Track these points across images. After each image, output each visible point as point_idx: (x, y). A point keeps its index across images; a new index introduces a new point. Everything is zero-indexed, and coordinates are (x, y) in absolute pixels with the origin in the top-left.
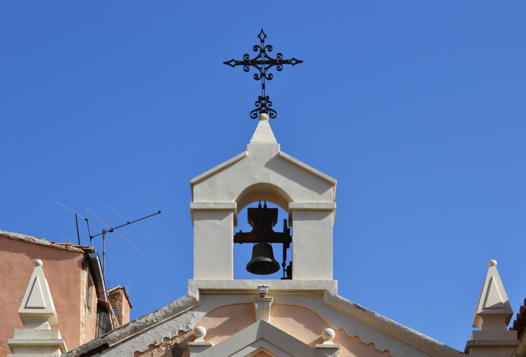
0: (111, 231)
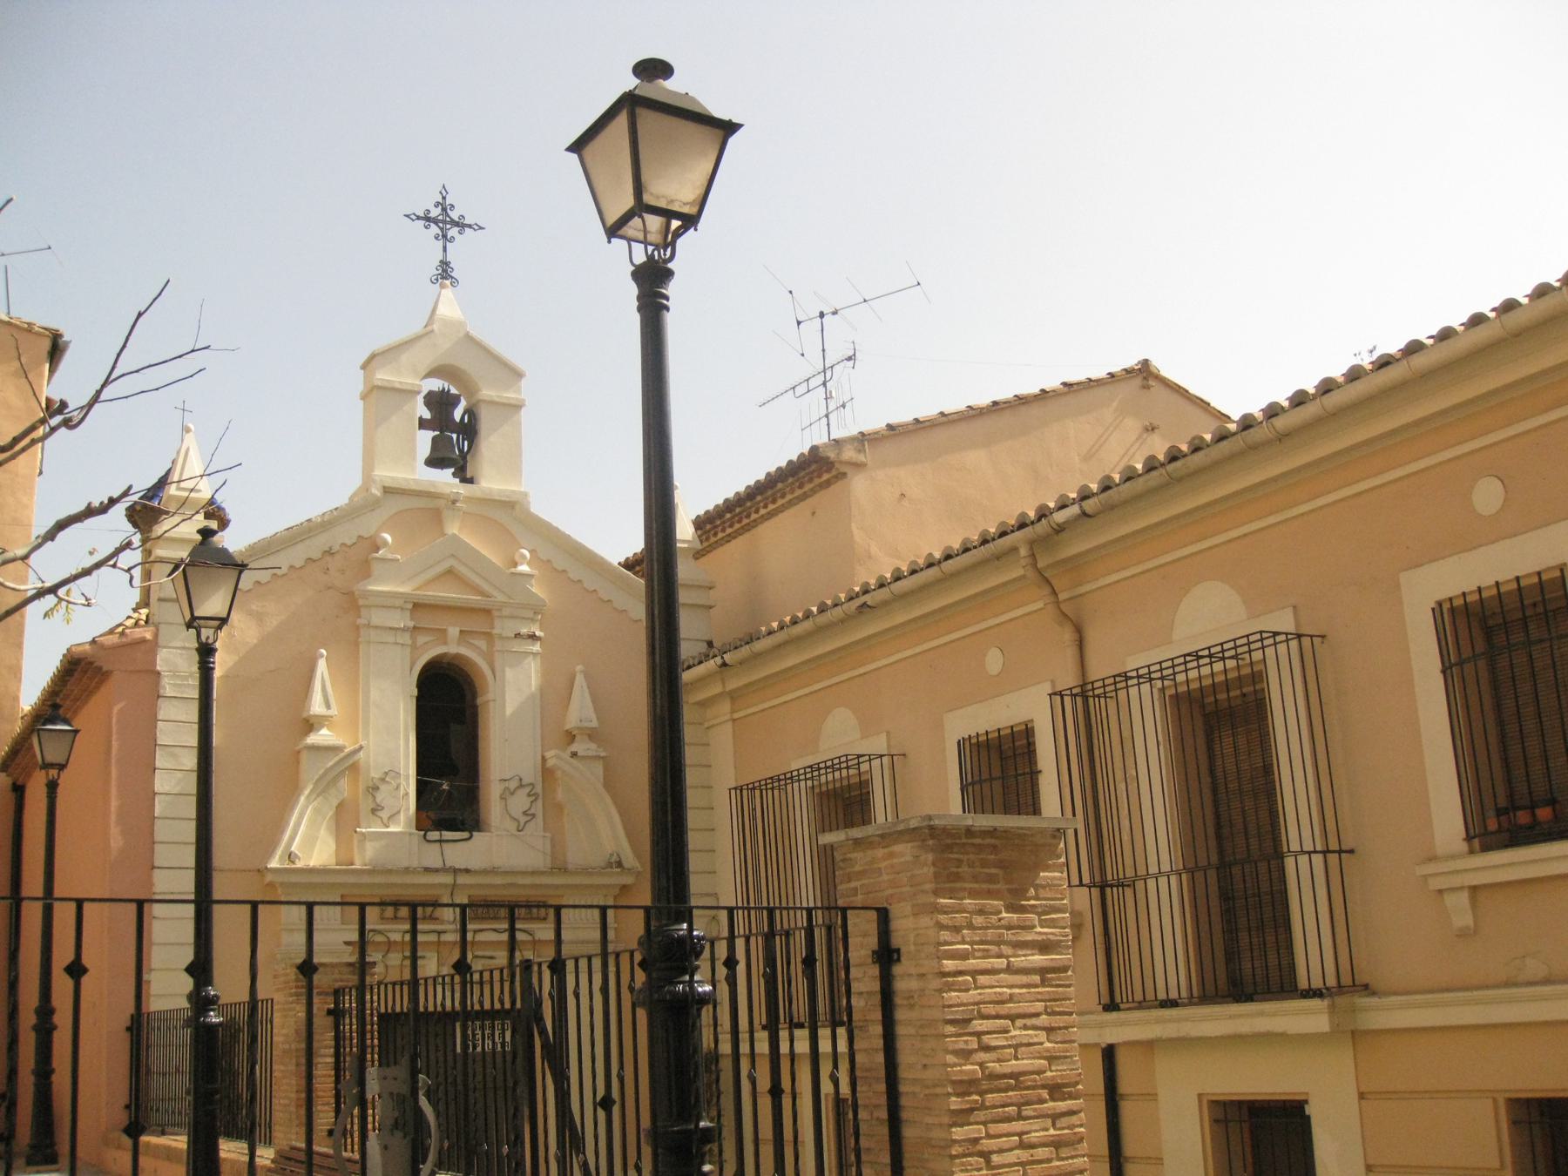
0: (835, 313)
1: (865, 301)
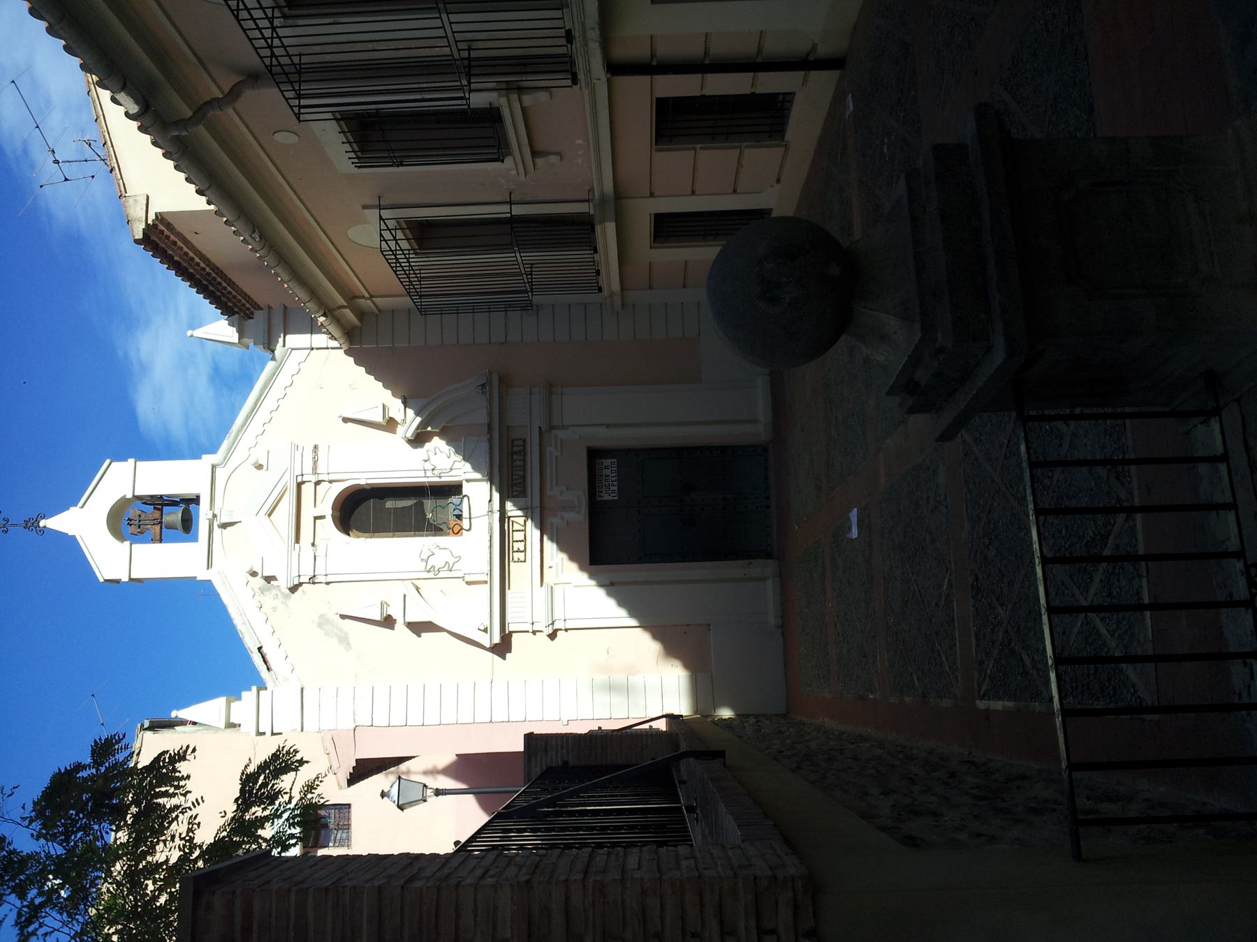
1: (37, 127)
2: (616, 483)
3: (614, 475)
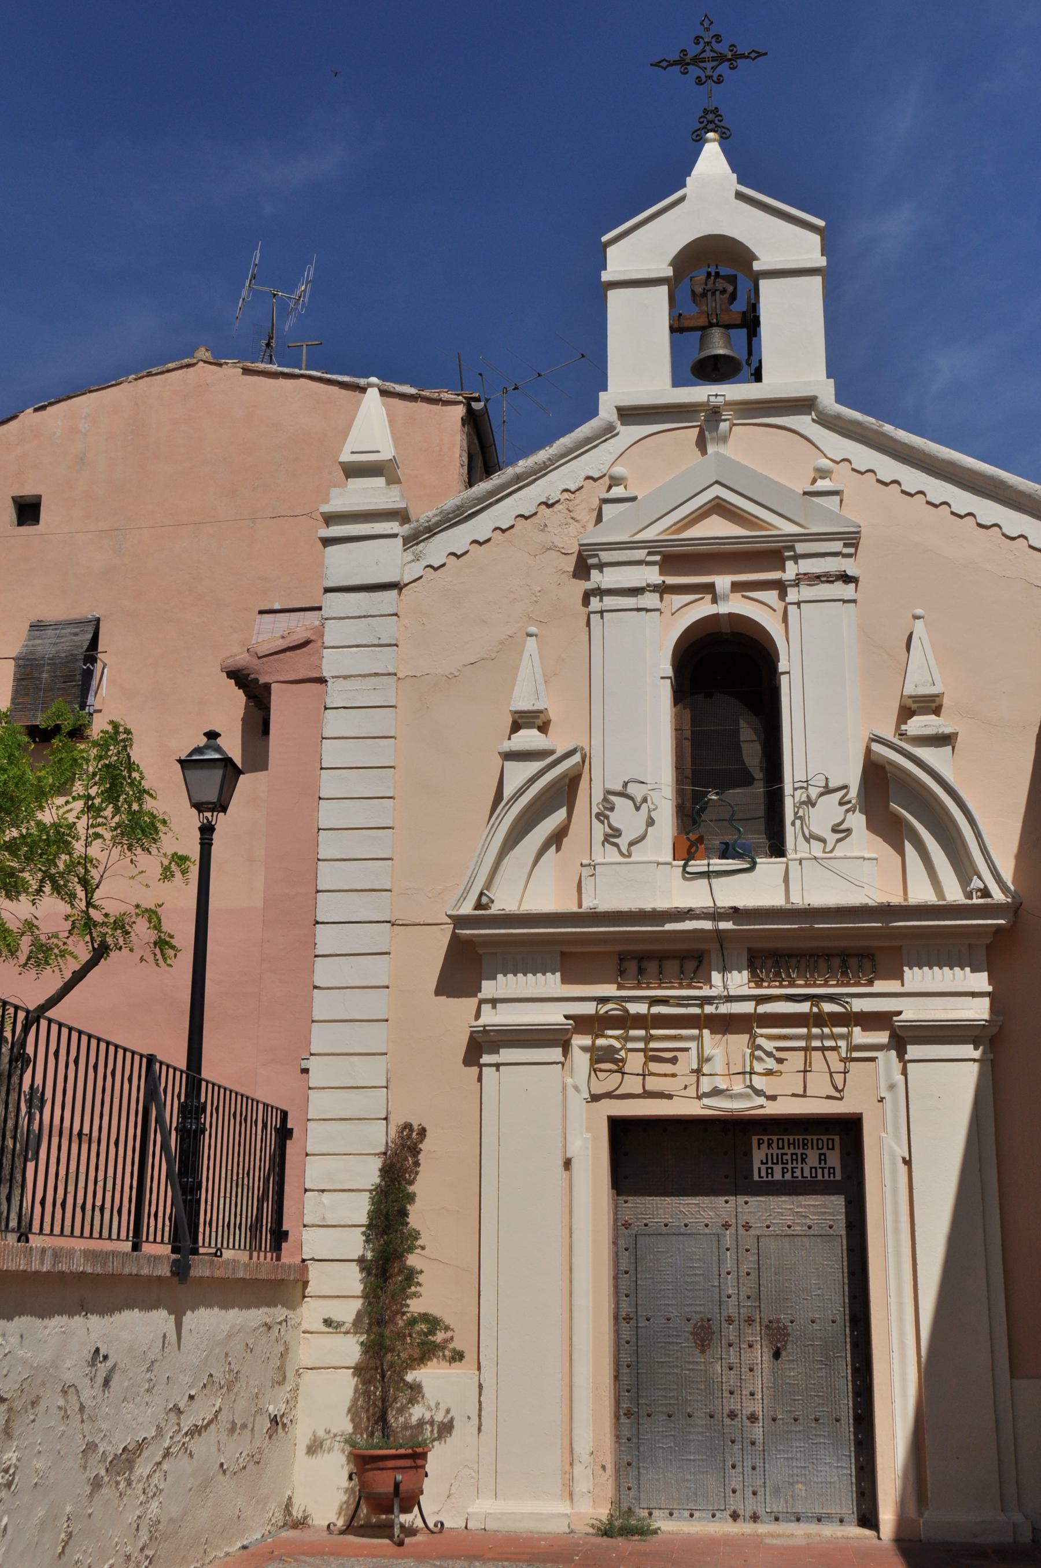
2: (788, 1176)
3: (807, 1173)
